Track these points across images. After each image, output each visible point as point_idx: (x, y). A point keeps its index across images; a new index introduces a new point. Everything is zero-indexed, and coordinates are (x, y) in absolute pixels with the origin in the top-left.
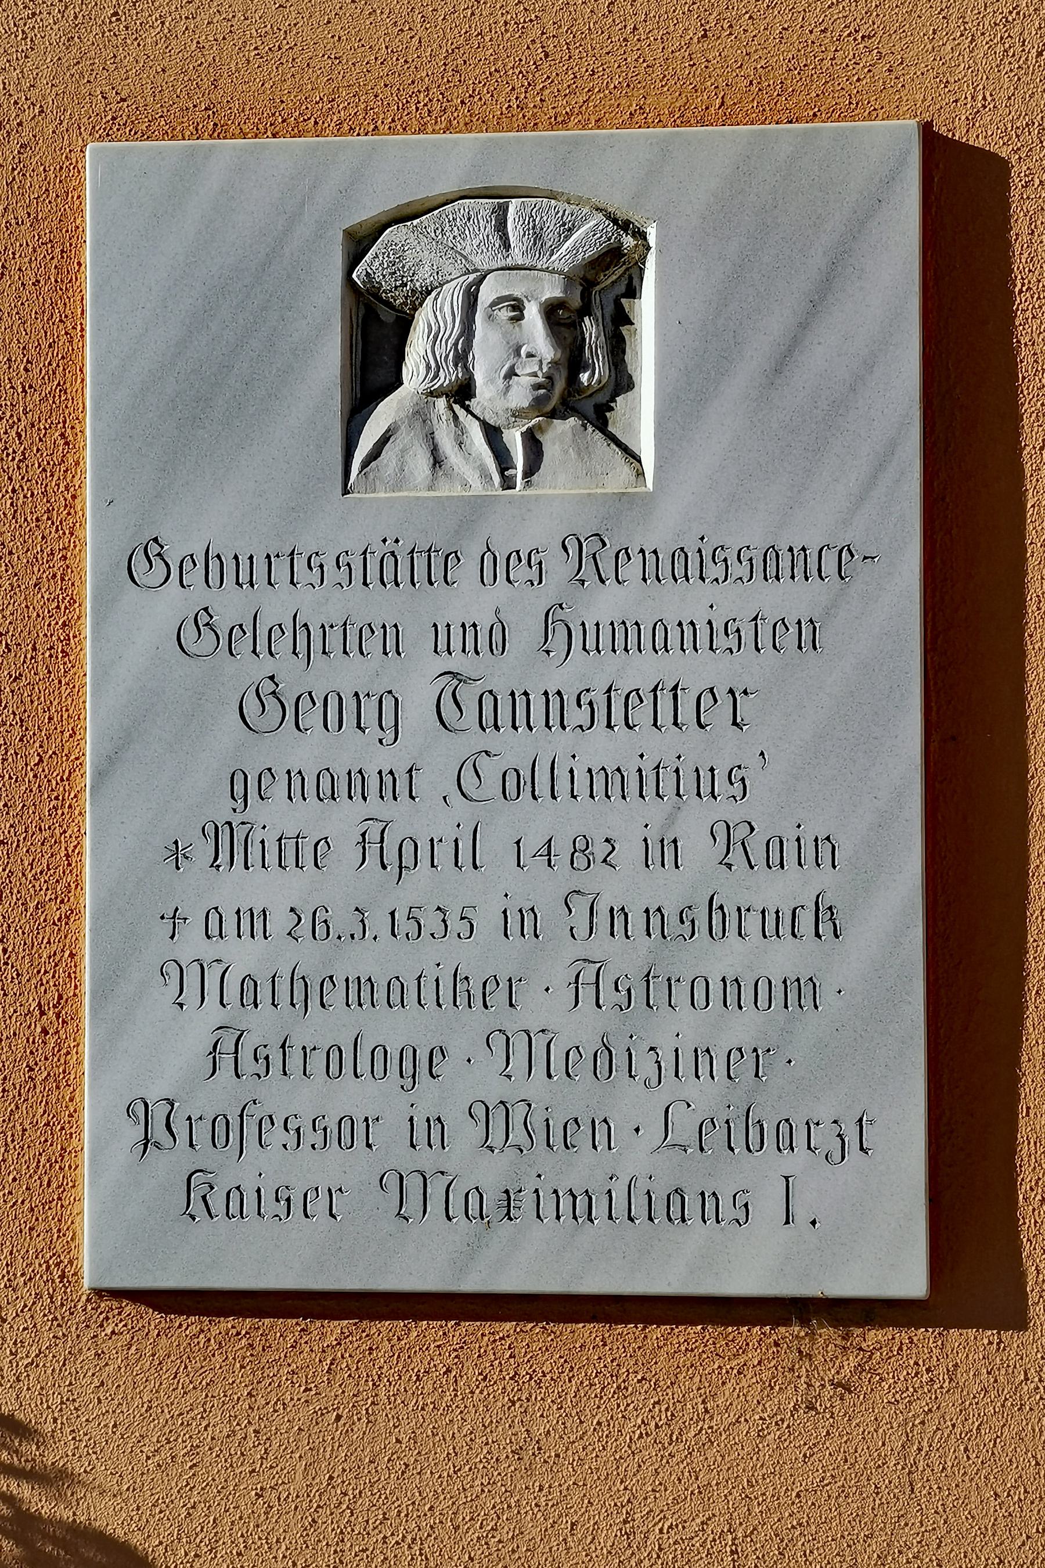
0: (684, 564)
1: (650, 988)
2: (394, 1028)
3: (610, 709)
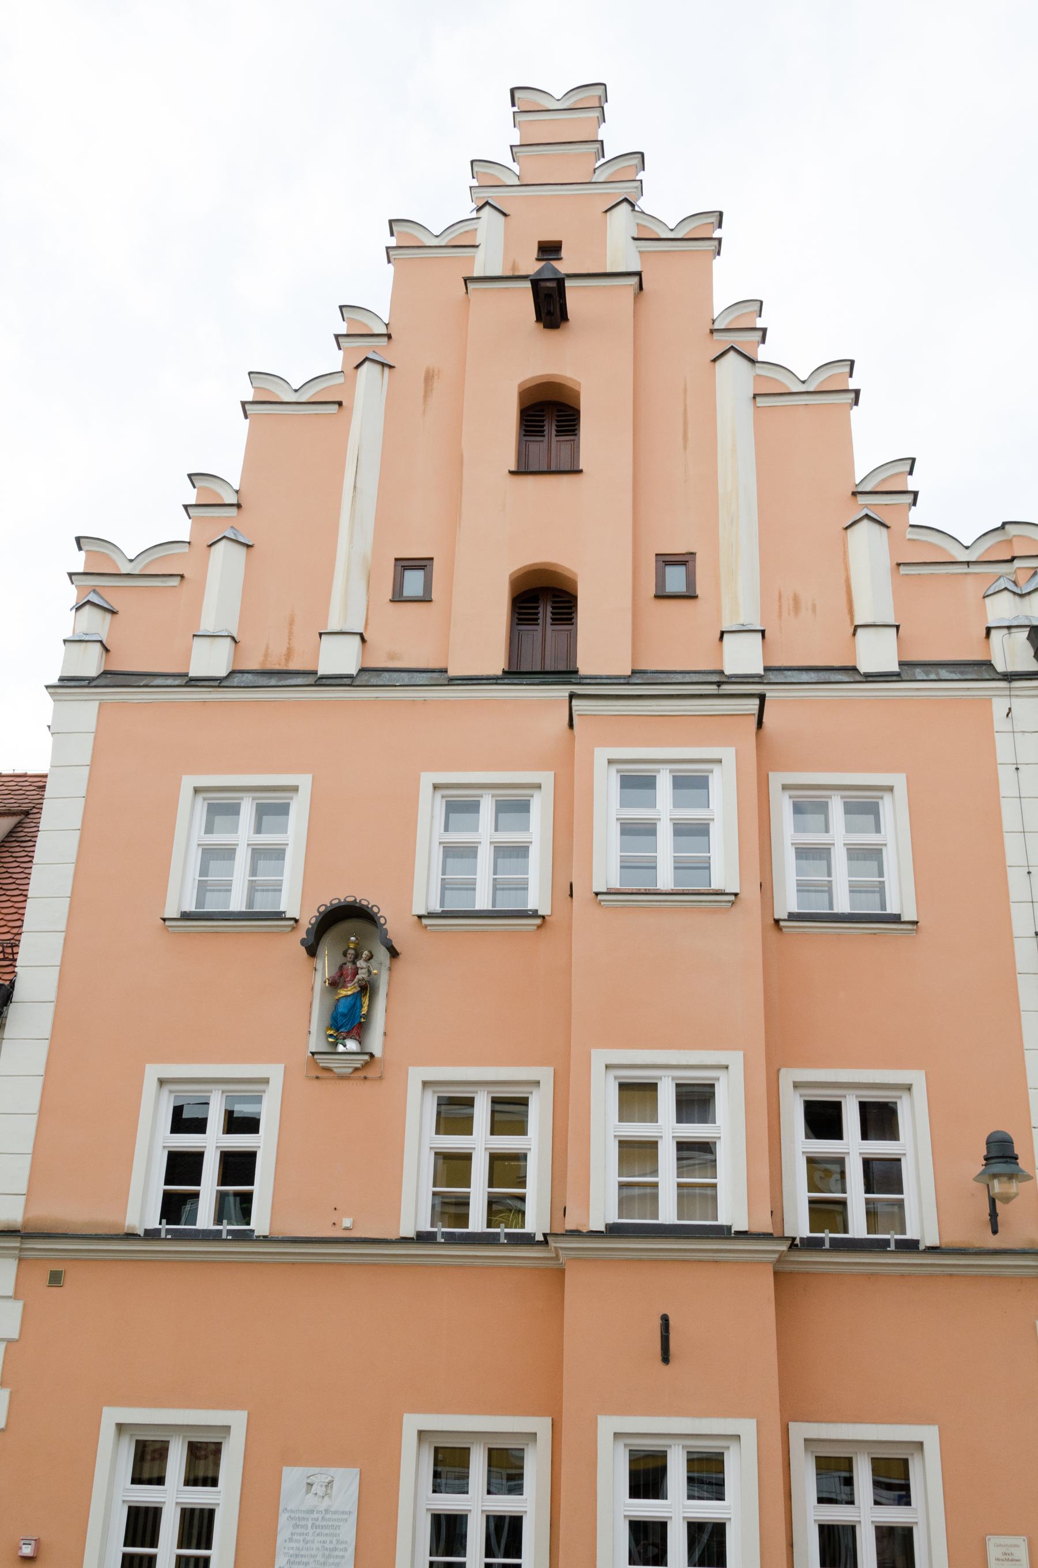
0: (335, 1513)
1: (329, 1556)
2: (304, 1560)
3: (326, 1527)
